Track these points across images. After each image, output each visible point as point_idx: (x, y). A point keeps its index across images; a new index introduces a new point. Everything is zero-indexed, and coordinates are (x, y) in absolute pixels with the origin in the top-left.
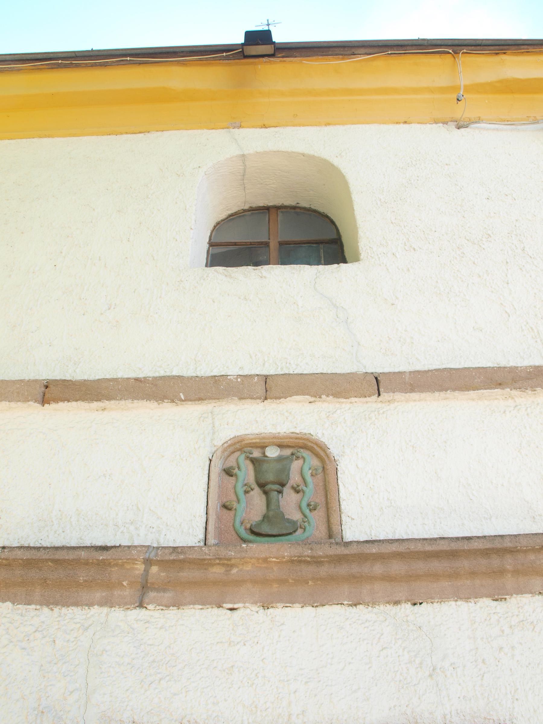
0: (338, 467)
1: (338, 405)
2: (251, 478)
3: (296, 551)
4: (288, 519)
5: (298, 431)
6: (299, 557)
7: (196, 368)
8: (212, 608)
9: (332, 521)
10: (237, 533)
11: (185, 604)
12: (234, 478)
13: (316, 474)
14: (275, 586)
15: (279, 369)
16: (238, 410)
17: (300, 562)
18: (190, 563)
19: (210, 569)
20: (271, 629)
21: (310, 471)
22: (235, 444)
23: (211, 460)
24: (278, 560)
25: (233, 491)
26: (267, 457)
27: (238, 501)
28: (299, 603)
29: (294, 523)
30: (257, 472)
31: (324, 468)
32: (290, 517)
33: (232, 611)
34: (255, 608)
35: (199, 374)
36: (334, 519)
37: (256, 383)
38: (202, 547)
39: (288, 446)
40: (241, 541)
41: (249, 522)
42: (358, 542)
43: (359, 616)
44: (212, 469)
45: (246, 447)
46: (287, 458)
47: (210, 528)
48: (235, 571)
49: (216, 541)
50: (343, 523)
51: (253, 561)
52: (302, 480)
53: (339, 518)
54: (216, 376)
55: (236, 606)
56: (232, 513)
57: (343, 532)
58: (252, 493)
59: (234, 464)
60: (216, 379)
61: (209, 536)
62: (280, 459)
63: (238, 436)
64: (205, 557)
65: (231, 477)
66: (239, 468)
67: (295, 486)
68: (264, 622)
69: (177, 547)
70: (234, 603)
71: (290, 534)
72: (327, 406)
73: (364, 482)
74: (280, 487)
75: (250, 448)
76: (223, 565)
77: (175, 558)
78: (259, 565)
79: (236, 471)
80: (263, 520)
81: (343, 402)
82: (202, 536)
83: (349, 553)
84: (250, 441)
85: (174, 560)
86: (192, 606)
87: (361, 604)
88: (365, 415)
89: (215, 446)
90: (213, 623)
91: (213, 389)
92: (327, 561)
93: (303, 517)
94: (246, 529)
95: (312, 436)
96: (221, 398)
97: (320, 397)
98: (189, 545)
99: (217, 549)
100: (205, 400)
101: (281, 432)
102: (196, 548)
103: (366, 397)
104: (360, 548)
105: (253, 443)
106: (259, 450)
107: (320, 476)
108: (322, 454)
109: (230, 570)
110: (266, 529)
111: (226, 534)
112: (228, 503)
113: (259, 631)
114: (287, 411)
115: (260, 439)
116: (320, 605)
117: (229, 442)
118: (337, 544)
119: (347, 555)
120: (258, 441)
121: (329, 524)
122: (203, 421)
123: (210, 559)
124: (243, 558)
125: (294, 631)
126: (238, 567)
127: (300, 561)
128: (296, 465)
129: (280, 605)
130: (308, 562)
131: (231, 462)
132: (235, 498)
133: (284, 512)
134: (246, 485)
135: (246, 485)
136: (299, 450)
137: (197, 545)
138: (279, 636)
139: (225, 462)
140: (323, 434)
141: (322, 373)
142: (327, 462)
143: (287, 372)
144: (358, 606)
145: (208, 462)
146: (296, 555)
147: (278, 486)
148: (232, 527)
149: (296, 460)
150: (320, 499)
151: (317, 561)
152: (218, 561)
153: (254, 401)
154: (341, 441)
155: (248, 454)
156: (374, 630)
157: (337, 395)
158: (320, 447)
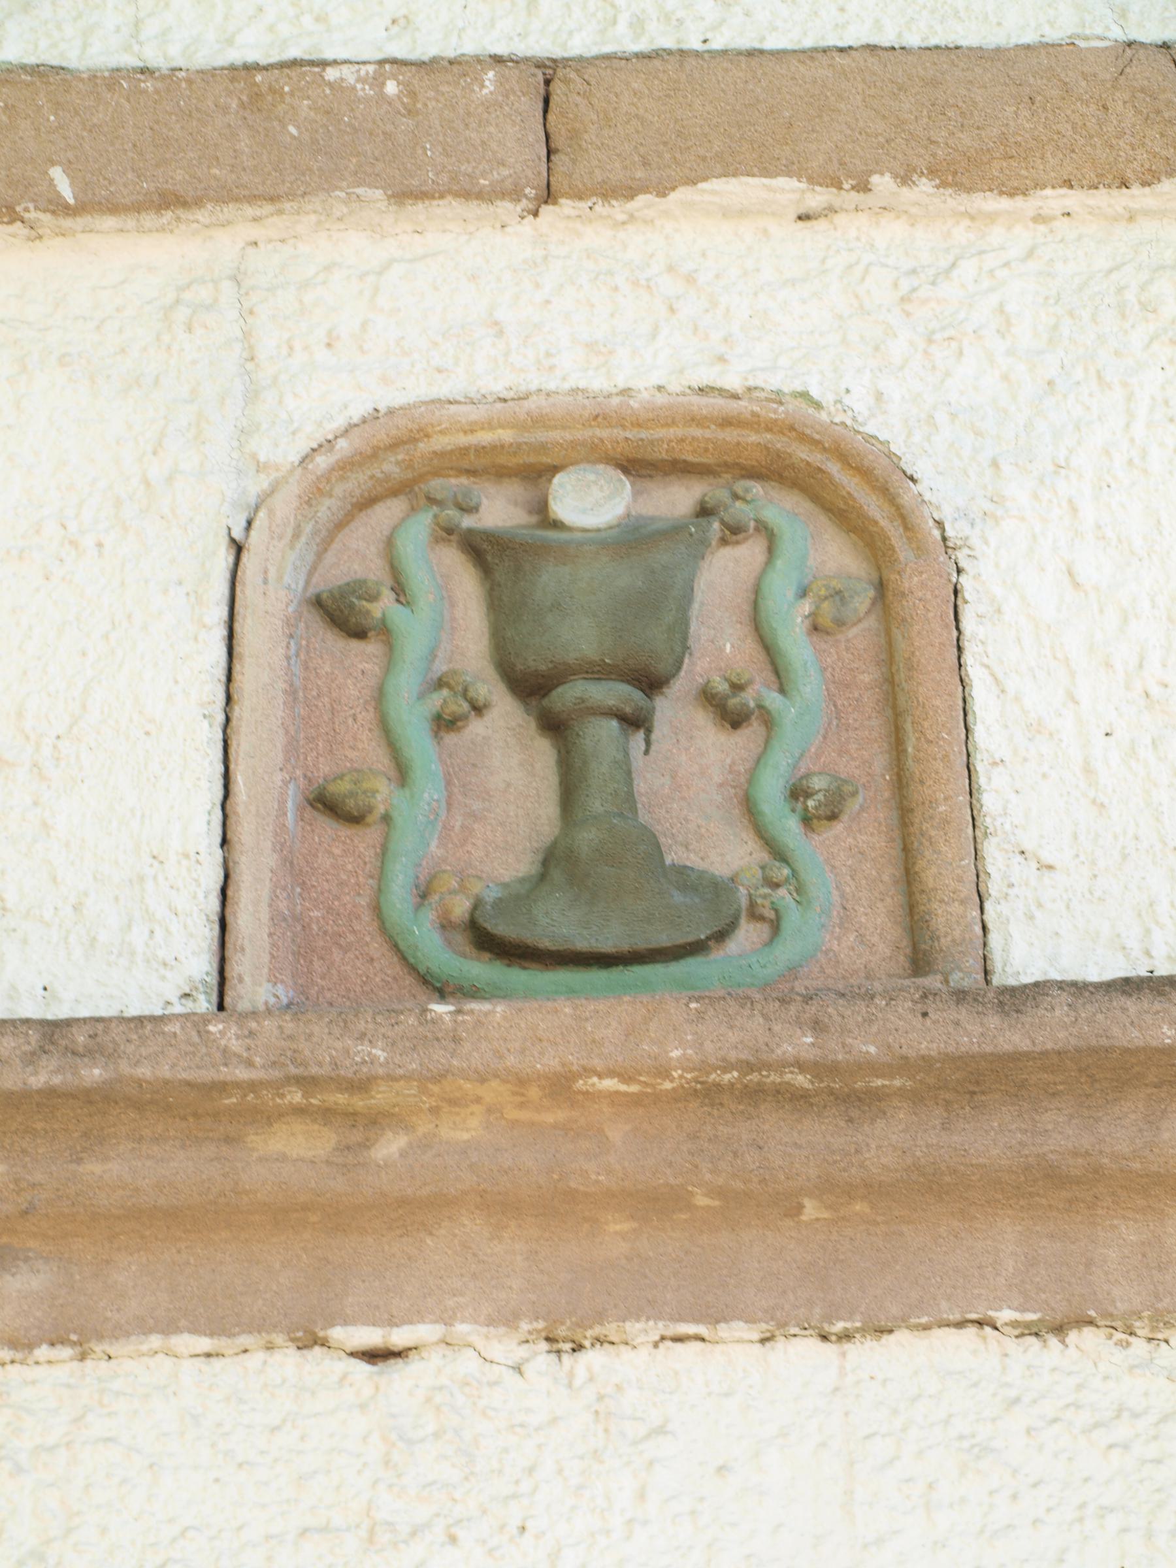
0: (963, 579)
1: (961, 233)
2: (470, 646)
3: (733, 1037)
4: (682, 871)
5: (732, 381)
6: (748, 1067)
7: (137, 23)
8: (270, 1347)
9: (929, 876)
10: (396, 948)
11: (119, 1332)
12: (372, 647)
13: (840, 623)
14: (618, 1225)
15: (622, 27)
16: (391, 262)
17: (754, 1095)
18: (138, 1106)
19: (254, 1139)
20: (596, 1454)
21: (806, 607)
22: (374, 455)
23: (238, 548)
24: (634, 1088)
25: (367, 717)
26: (557, 525)
27: (402, 773)
28: (750, 1320)
29: (716, 890)
30: (504, 610)
31: (881, 586)
32: (692, 860)
33: (381, 1367)
34: (504, 1347)
35: (153, 56)
36: (943, 869)
37: (488, 105)
38: (205, 1019)
39: (679, 469)
40: (421, 992)
41: (462, 889)
42: (1078, 989)
43: (1080, 1387)
44: (248, 593)
45: (437, 473)
46: (673, 531)
47: (244, 921)
48: (390, 1147)
49: (280, 990)
50: (994, 887)
51: (493, 1092)
52: (761, 656)
53: (969, 861)
54: (256, 67)
55: (399, 1338)
56: (365, 840)
57: (994, 939)
58: (477, 728)
59: (373, 570)
60: (257, 87)
61: (239, 966)
62: (632, 539)
63: (391, 412)
64: (225, 1073)
65: (355, 645)
66: (400, 591)
67: (722, 687)
68: (554, 1421)
69: (68, 1023)
70: (392, 1322)
71: (695, 948)
72: (902, 236)
73: (1109, 665)
74: (637, 695)
75: (464, 480)
76: (327, 1115)
77: (57, 1080)
78: (524, 1115)
79: (385, 606)
80: (543, 877)
81: (992, 217)
82: (199, 965)
83: (1025, 1045)
84: (463, 440)
85: (51, 1093)
86: (155, 1341)
87: (1091, 1322)
88: (1120, 290)
89: (261, 467)
90: (275, 1429)
91: (244, 143)
92: (901, 1093)
93: (763, 856)
94: (446, 925)
95: (818, 406)
96: (291, 196)
97: (863, 187)
98: (132, 1012)
99: (290, 1027)
100: (198, 202)
101: (639, 384)
102: (174, 1028)
103: (1125, 184)
104: (1090, 1021)
105: (481, 450)
106: (515, 489)
107: (861, 634)
108: (873, 507)
109: (366, 1145)
110: (557, 922)
111: (337, 955)
112: (342, 787)
113: (531, 1470)
114: (671, 269)
115: (520, 426)
116: (863, 1331)
117: (342, 443)
118: (961, 996)
119: (1016, 1057)
120: (506, 436)
121: (910, 894)
122: (190, 329)
123: (253, 1086)
124: (440, 1077)
125: (721, 1469)
126: (409, 1128)
127: (752, 1091)
128: (722, 573)
129: (643, 1330)
130: (798, 1099)
131: (356, 559)
132: (379, 758)
133: (657, 829)
134: (440, 683)
135: (440, 683)
136: (740, 486)
137: (177, 1009)
138: (642, 1496)
139: (320, 556)
140: (879, 396)
141: (872, 48)
142: (904, 553)
143: (668, 43)
144: (1073, 1336)
145: (223, 559)
146: (733, 1056)
147: (624, 689)
148: (366, 917)
149: (724, 542)
150: (864, 762)
151: (845, 1093)
152: (296, 1097)
153: (483, 209)
154: (978, 434)
155: (451, 513)
156: (1158, 1461)
157: (958, 173)
158: (865, 472)
